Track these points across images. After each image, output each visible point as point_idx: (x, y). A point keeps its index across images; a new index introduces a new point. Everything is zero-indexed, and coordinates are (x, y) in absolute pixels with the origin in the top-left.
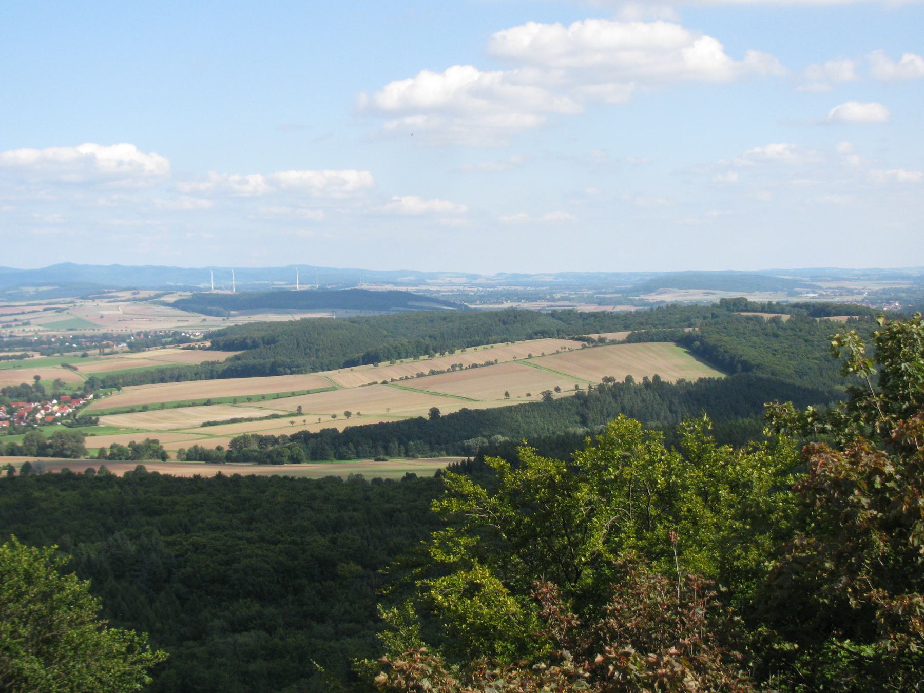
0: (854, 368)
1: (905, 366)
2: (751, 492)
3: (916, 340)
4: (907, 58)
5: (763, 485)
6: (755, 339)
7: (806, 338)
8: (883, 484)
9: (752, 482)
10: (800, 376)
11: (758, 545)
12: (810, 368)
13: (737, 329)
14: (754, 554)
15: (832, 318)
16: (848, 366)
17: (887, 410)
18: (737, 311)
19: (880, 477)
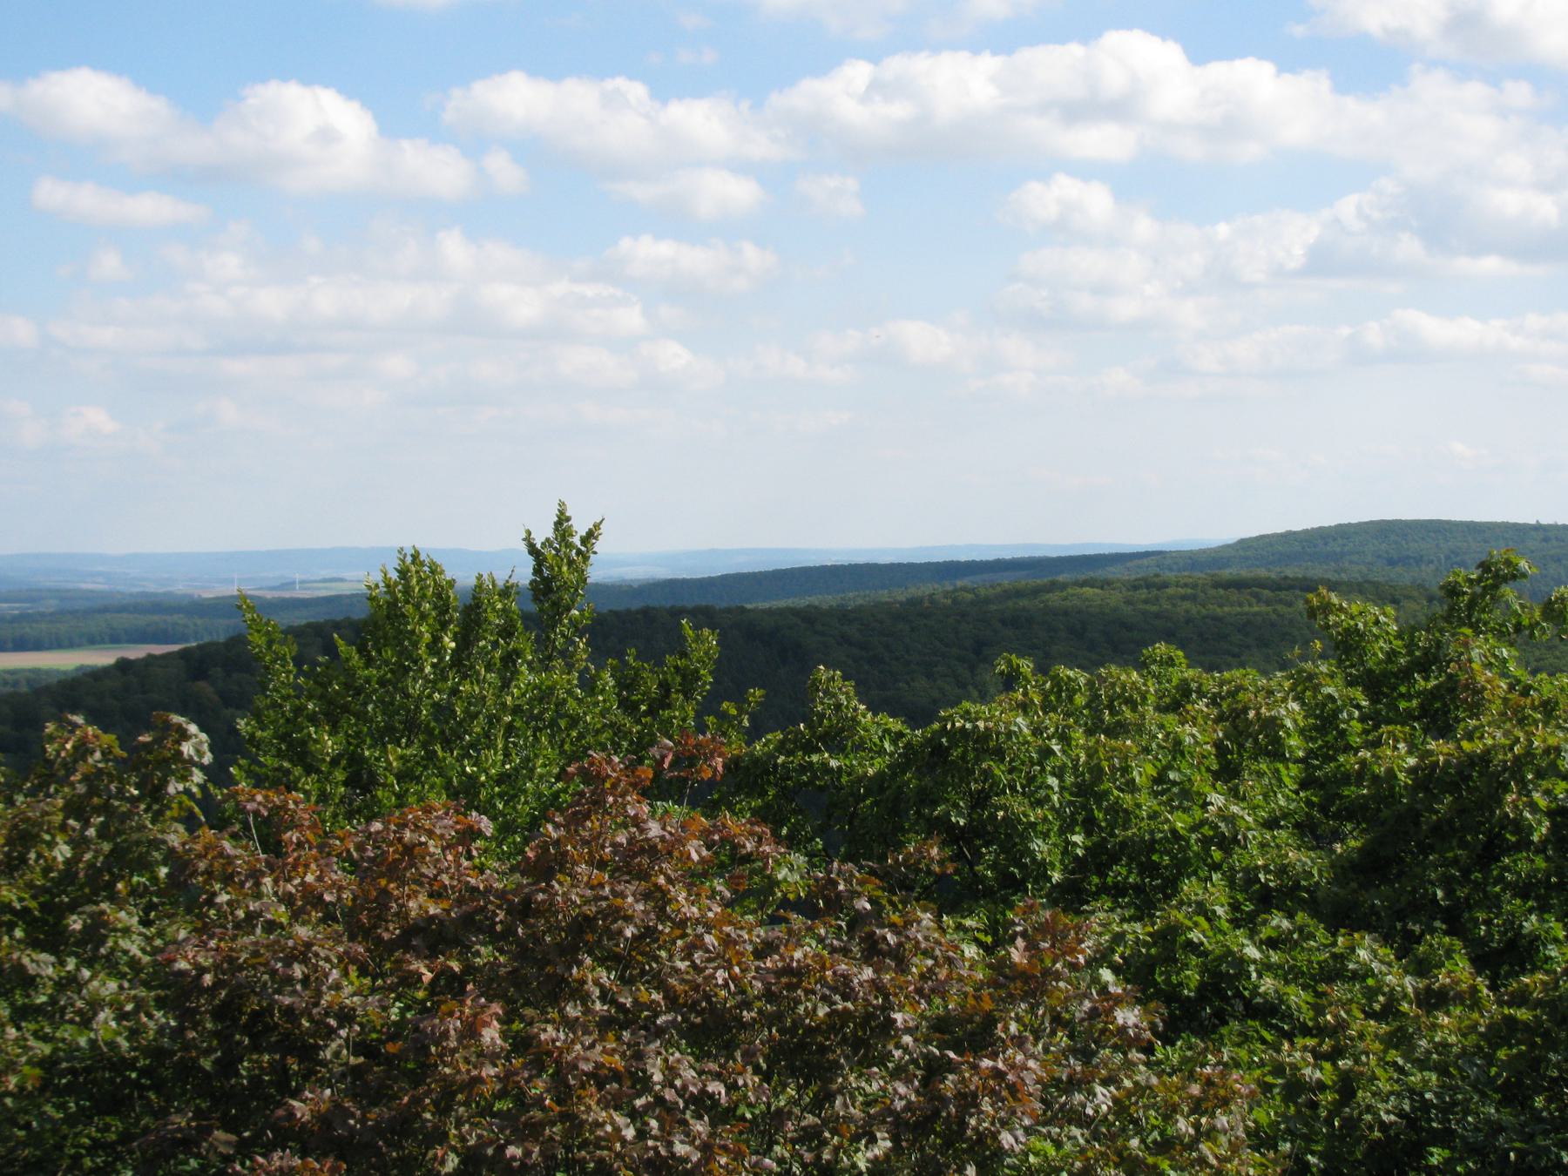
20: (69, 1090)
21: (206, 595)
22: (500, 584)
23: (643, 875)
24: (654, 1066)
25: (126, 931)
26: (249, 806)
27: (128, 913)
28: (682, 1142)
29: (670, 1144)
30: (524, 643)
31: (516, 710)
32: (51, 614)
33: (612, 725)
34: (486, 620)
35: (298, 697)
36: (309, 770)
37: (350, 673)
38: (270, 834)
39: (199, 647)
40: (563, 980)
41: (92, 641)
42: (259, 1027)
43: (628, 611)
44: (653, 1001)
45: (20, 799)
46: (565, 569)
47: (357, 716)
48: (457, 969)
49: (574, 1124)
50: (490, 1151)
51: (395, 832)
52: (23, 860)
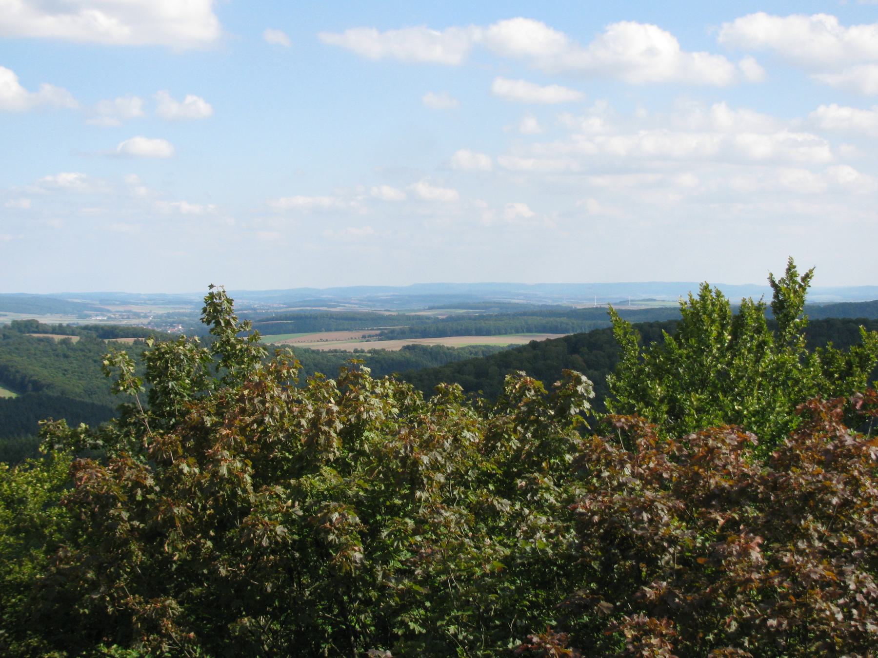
0: (124, 387)
1: (172, 385)
2: (25, 508)
3: (183, 360)
4: (190, 99)
5: (38, 501)
6: (45, 359)
7: (95, 358)
8: (143, 496)
9: (27, 498)
10: (89, 395)
11: (32, 559)
12: (98, 388)
13: (28, 350)
14: (28, 567)
15: (120, 340)
16: (118, 385)
17: (154, 425)
18: (29, 332)
19: (141, 490)
20: (519, 574)
21: (578, 307)
22: (756, 303)
23: (844, 469)
24: (850, 580)
25: (548, 489)
26: (618, 424)
27: (549, 479)
28: (872, 624)
29: (864, 625)
30: (769, 338)
31: (763, 375)
32: (496, 316)
33: (818, 385)
34: (747, 324)
35: (640, 364)
36: (647, 405)
37: (670, 352)
38: (628, 439)
39: (575, 335)
40: (796, 527)
41: (517, 331)
42: (626, 544)
43: (818, 321)
44: (850, 542)
45: (491, 416)
46: (792, 295)
47: (674, 375)
48: (737, 518)
49: (808, 610)
50: (757, 621)
51: (703, 440)
52: (494, 447)
